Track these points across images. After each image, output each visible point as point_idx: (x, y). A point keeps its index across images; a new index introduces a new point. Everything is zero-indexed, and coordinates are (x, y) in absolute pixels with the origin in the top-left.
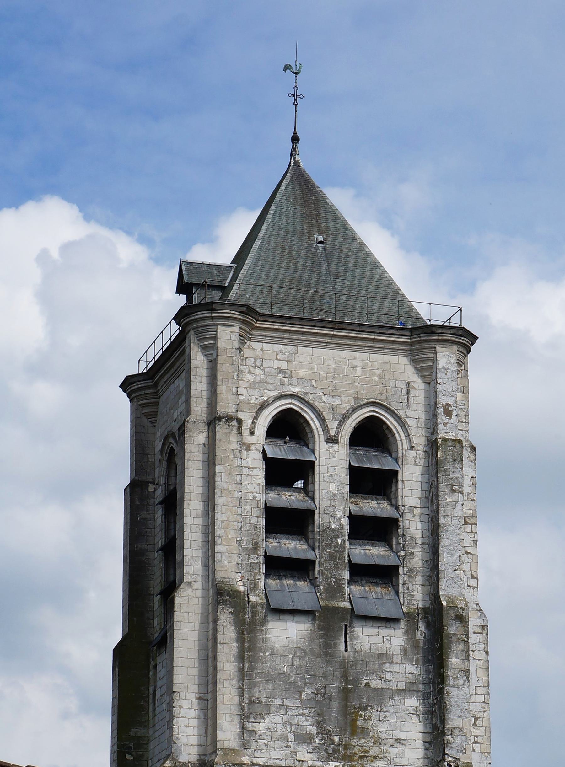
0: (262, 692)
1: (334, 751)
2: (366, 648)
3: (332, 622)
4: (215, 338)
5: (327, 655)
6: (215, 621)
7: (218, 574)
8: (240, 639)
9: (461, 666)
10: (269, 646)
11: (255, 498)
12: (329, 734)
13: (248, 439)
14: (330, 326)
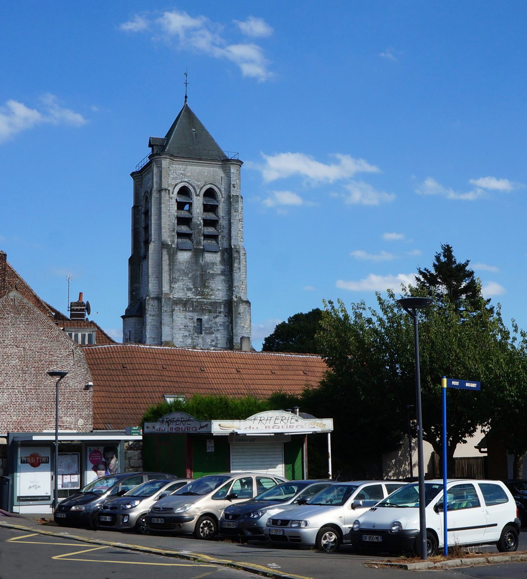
0: (176, 275)
1: (199, 293)
2: (208, 261)
3: (198, 253)
4: (161, 164)
5: (196, 263)
6: (162, 253)
7: (163, 239)
8: (169, 259)
12: (197, 288)
13: (172, 195)
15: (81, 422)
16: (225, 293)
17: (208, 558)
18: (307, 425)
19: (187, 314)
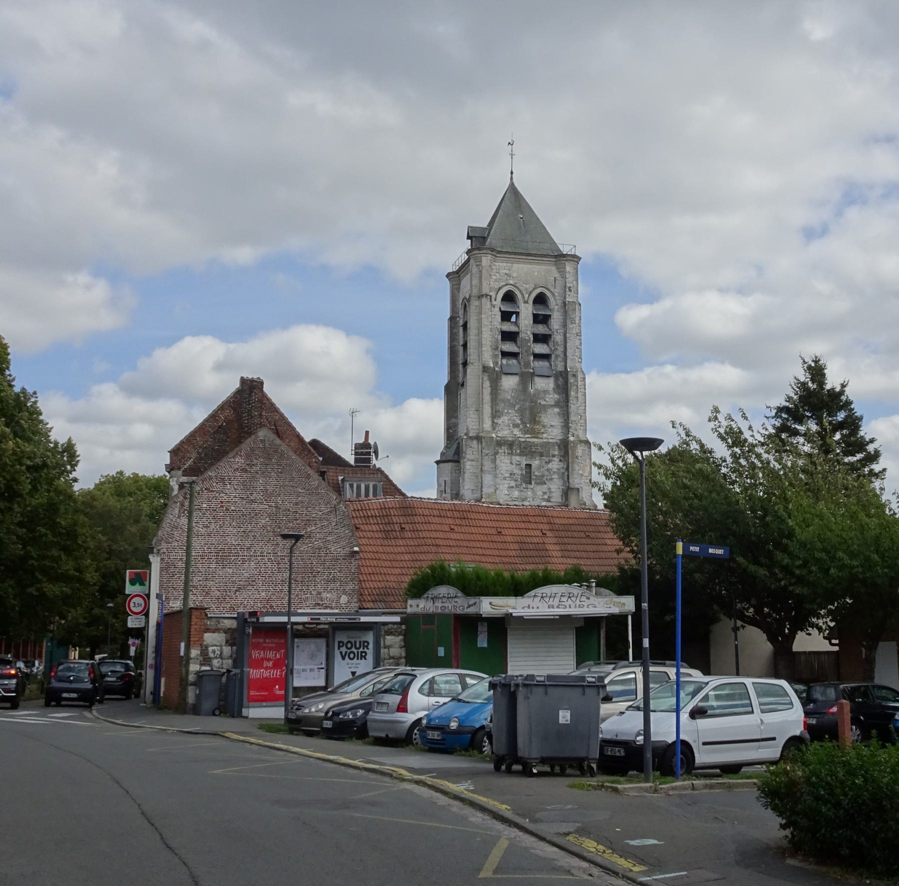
0: (501, 406)
3: (527, 378)
13: (494, 303)
15: (344, 599)
16: (560, 431)
17: (404, 772)
18: (602, 603)
19: (514, 457)
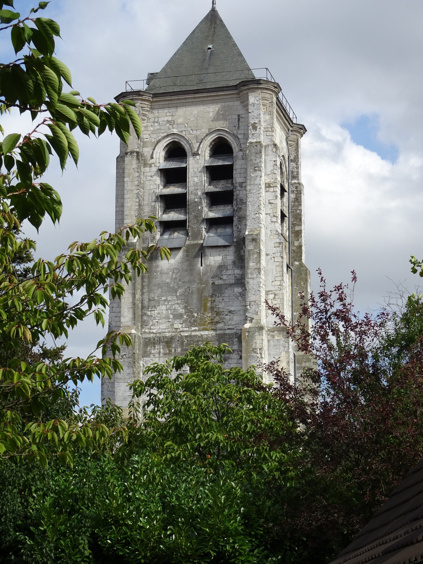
1: (195, 321)
9: (256, 267)
10: (159, 269)
11: (154, 192)
12: (192, 312)
14: (210, 90)
